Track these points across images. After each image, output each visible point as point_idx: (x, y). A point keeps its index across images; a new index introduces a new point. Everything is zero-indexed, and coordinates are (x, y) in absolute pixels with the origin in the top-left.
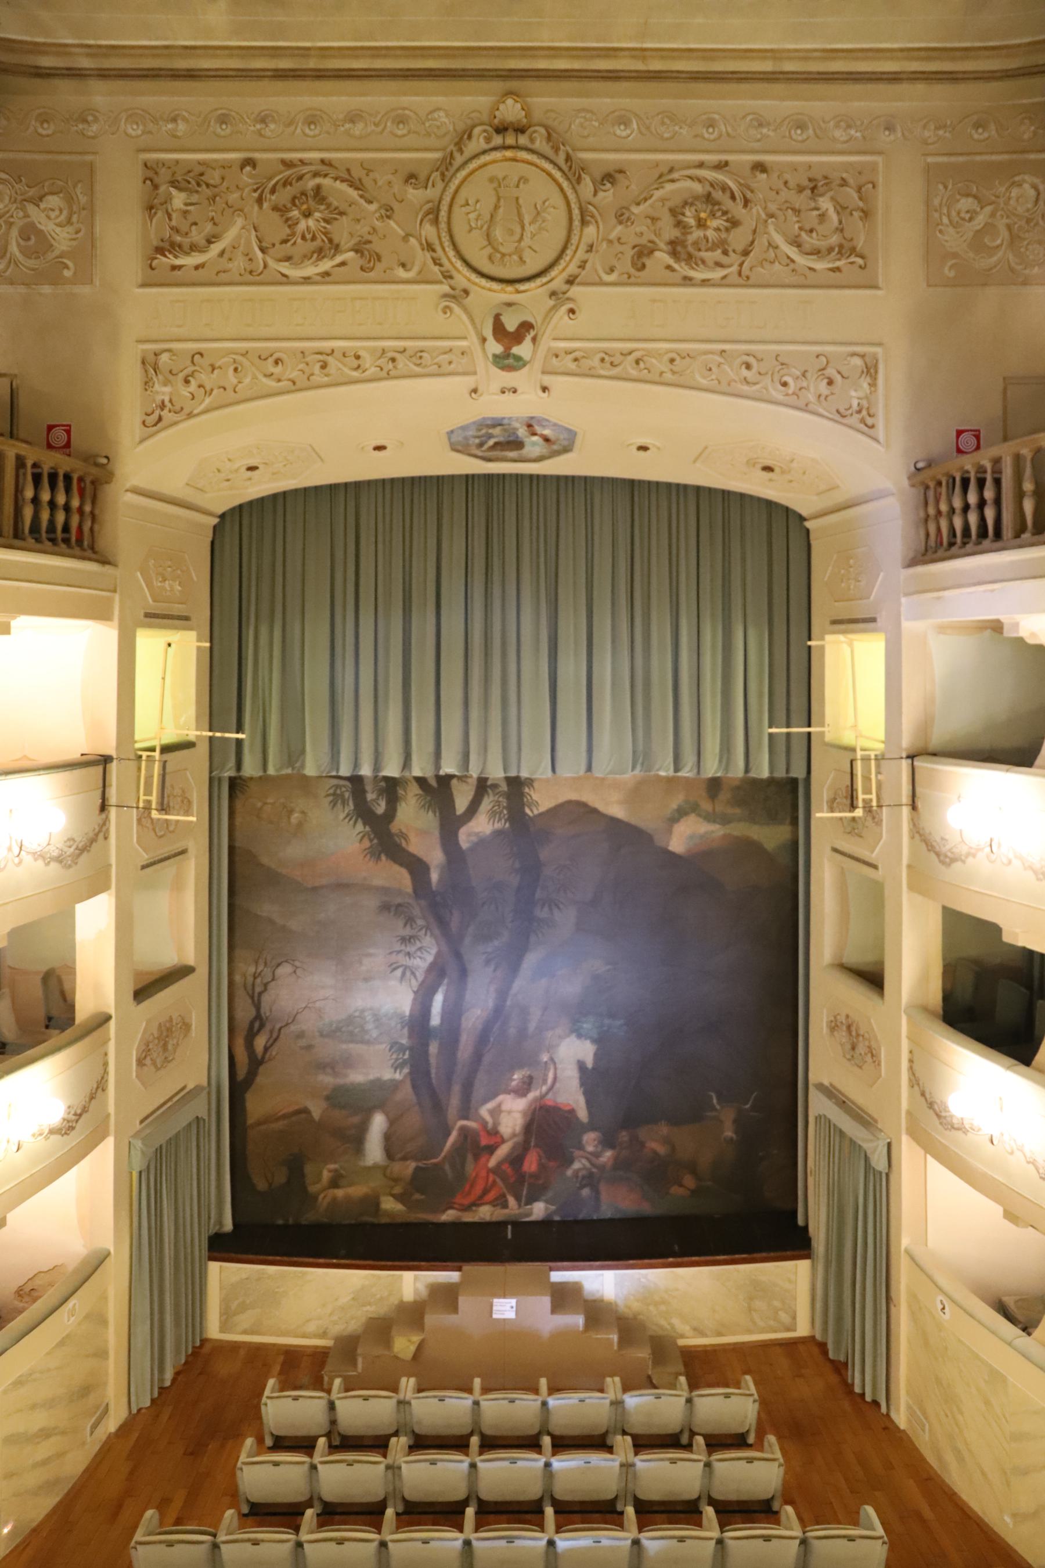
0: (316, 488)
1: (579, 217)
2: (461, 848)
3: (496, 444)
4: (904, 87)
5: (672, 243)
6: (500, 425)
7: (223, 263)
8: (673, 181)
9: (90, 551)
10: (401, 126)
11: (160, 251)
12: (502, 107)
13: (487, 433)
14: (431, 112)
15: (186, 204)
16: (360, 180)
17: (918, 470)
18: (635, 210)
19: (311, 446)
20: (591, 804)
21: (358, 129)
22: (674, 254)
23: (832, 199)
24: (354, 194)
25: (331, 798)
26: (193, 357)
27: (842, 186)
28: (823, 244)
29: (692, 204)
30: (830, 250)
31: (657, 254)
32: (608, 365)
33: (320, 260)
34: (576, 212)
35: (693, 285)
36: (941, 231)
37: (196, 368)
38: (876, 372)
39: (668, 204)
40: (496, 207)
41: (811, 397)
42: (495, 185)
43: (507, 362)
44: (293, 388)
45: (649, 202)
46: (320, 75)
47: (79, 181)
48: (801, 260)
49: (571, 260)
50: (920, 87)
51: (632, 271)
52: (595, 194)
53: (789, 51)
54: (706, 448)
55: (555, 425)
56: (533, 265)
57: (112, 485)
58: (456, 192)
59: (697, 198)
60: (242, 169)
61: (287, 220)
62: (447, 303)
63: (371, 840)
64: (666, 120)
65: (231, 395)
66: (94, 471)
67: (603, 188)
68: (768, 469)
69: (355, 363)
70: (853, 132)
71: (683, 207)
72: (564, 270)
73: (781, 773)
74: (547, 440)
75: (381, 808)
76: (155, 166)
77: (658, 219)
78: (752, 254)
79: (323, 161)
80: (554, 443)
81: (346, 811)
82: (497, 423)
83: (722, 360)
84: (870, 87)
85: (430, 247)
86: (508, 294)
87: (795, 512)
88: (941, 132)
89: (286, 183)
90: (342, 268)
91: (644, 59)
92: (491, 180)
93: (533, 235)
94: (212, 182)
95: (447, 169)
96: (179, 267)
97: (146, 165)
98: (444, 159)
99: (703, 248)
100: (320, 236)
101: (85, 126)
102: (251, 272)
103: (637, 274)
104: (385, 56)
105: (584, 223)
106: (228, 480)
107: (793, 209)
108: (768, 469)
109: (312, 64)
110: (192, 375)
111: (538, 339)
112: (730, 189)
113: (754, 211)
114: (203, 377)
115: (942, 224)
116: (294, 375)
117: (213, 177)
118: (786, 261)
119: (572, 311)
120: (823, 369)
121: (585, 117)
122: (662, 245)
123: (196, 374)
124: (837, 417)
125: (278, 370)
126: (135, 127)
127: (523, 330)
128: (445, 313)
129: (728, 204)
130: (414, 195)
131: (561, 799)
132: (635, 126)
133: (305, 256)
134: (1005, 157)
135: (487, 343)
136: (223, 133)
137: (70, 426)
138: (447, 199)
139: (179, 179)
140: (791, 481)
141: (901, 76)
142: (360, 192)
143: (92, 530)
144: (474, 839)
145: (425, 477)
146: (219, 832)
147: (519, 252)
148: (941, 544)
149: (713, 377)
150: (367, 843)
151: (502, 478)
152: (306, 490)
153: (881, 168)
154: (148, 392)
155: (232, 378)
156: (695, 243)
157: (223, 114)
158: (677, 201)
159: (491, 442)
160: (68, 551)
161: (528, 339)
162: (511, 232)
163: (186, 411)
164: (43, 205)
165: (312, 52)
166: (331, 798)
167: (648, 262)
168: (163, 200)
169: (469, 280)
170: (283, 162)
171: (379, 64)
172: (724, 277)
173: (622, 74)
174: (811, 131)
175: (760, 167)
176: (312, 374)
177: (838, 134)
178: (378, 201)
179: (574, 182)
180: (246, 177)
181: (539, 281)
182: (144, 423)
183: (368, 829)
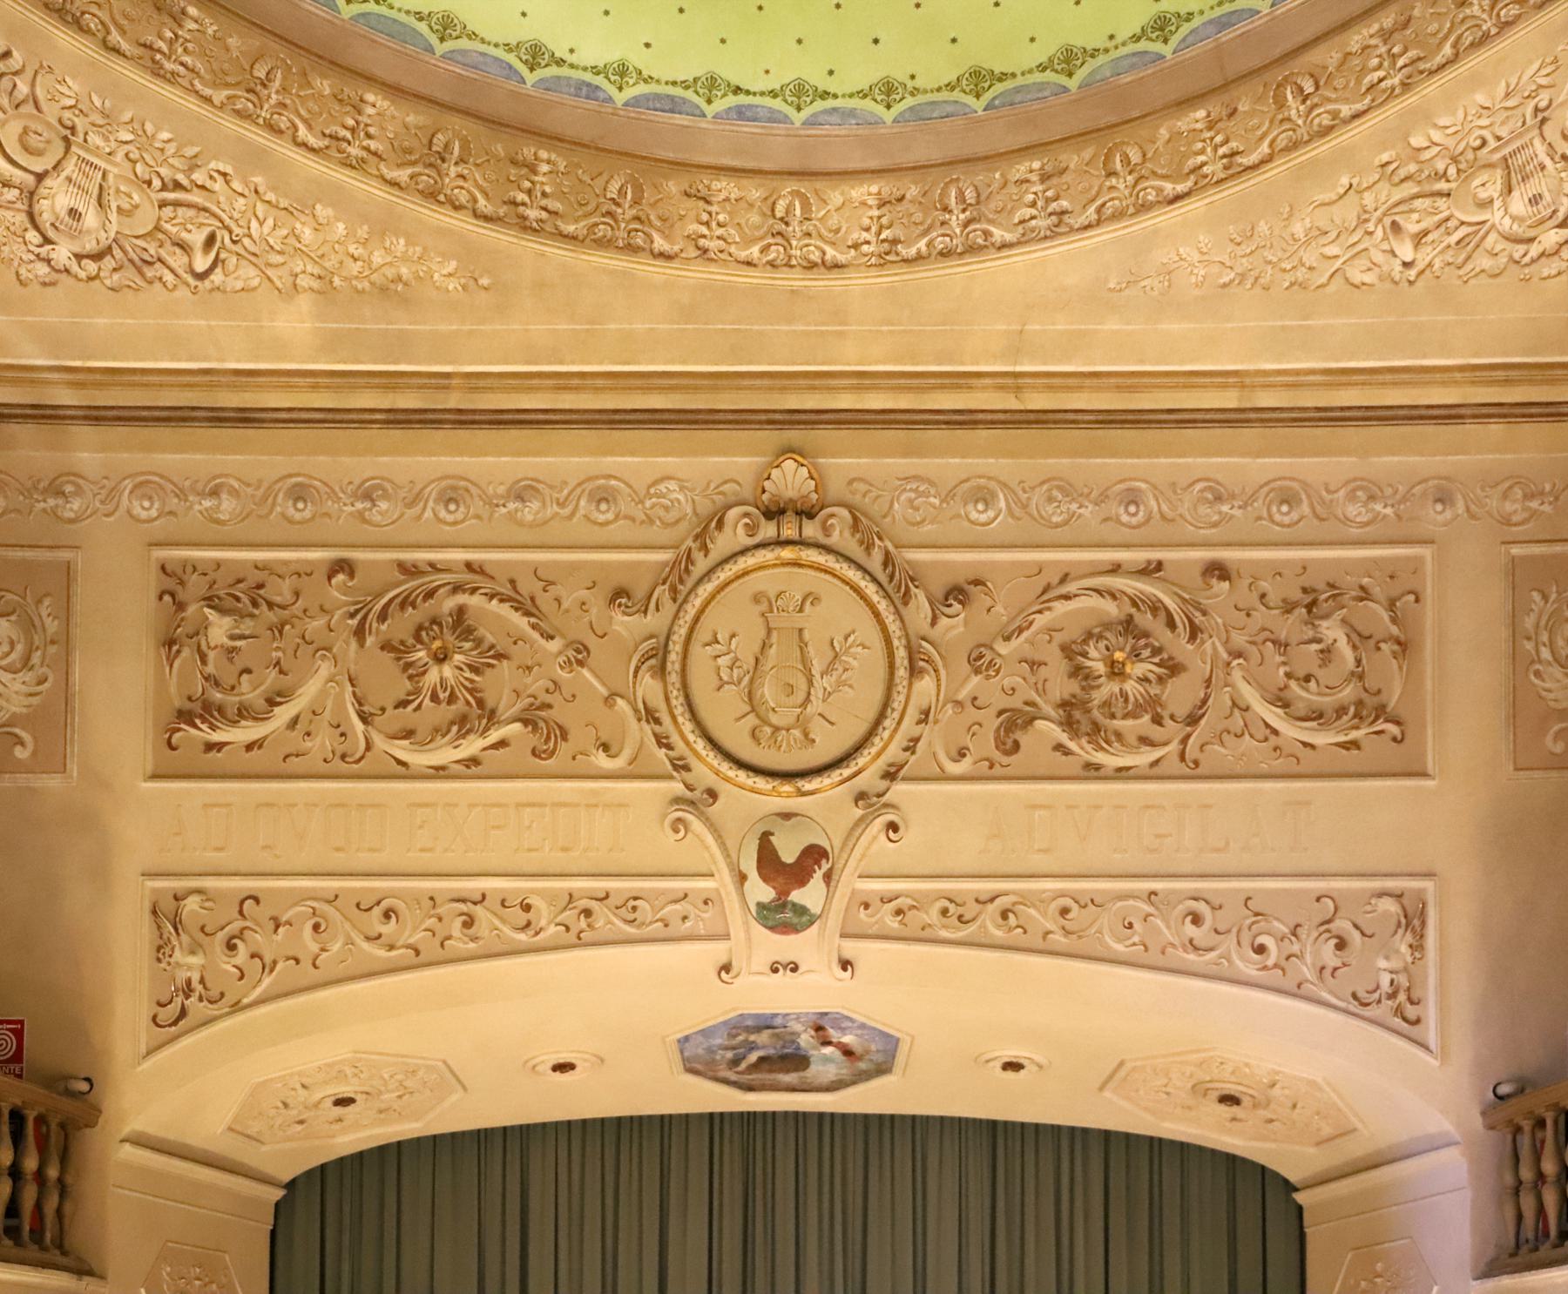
0: (455, 1138)
1: (906, 662)
3: (762, 1060)
4: (1471, 429)
5: (1064, 705)
6: (768, 1027)
7: (295, 740)
8: (1067, 597)
9: (57, 1252)
10: (603, 506)
11: (186, 717)
13: (746, 1041)
14: (655, 483)
15: (233, 638)
16: (532, 599)
17: (1500, 1098)
18: (1003, 648)
19: (445, 1062)
21: (530, 511)
22: (1069, 724)
23: (1344, 621)
24: (521, 622)
26: (242, 902)
27: (1362, 599)
28: (1327, 701)
29: (1100, 637)
30: (1341, 711)
31: (1039, 724)
32: (954, 920)
33: (464, 737)
34: (901, 654)
35: (1105, 778)
36: (1537, 674)
37: (248, 924)
38: (1423, 924)
39: (1059, 638)
41: (1308, 973)
42: (764, 607)
44: (416, 961)
45: (1025, 634)
46: (465, 419)
47: (46, 595)
48: (1291, 731)
49: (891, 737)
50: (1496, 429)
51: (997, 756)
52: (934, 622)
53: (1265, 373)
54: (1121, 1064)
55: (863, 1026)
56: (827, 745)
57: (97, 1129)
58: (697, 619)
59: (1107, 626)
60: (329, 579)
62: (680, 814)
64: (1057, 494)
65: (307, 973)
66: (67, 1105)
67: (947, 610)
68: (1229, 1099)
69: (523, 918)
70: (1378, 507)
71: (1085, 642)
72: (879, 754)
74: (848, 1052)
76: (179, 571)
78: (1203, 722)
79: (469, 566)
80: (860, 1058)
82: (764, 1024)
83: (1151, 909)
85: (651, 716)
86: (781, 797)
87: (1276, 1175)
88: (1534, 504)
89: (406, 602)
91: (1018, 389)
92: (757, 599)
93: (827, 695)
94: (278, 599)
95: (681, 581)
96: (219, 746)
97: (163, 568)
98: (676, 562)
99: (1119, 715)
100: (463, 694)
101: (60, 501)
102: (343, 757)
103: (1005, 760)
105: (914, 672)
106: (301, 1122)
107: (1274, 642)
108: (1229, 1099)
109: (454, 401)
110: (240, 935)
111: (835, 877)
112: (1166, 609)
113: (1208, 645)
114: (258, 939)
115: (1540, 661)
116: (417, 937)
117: (281, 591)
118: (1262, 732)
119: (893, 827)
120: (1328, 922)
121: (916, 490)
122: (1048, 710)
123: (246, 932)
124: (1353, 1006)
125: (388, 929)
126: (146, 504)
127: (810, 861)
128: (676, 831)
129: (1162, 635)
130: (624, 624)
132: (1002, 504)
133: (437, 730)
135: (747, 884)
136: (298, 516)
137: (21, 1022)
138: (681, 631)
139: (221, 593)
140: (1271, 1121)
141: (1463, 411)
142: (533, 620)
143: (59, 1212)
145: (641, 1118)
147: (802, 723)
148: (1547, 1235)
149: (1136, 939)
151: (770, 1119)
152: (435, 1139)
153: (1429, 567)
154: (163, 965)
156: (1106, 704)
157: (297, 485)
158: (1073, 633)
159: (753, 1057)
160: (15, 1251)
161: (818, 875)
162: (790, 689)
163: (230, 998)
165: (454, 382)
167: (1025, 739)
168: (191, 630)
169: (717, 773)
170: (402, 566)
171: (567, 401)
172: (1156, 763)
173: (981, 416)
174: (1305, 508)
175: (1217, 570)
176: (449, 938)
177: (1352, 510)
178: (563, 636)
179: (897, 602)
180: (337, 592)
181: (836, 776)
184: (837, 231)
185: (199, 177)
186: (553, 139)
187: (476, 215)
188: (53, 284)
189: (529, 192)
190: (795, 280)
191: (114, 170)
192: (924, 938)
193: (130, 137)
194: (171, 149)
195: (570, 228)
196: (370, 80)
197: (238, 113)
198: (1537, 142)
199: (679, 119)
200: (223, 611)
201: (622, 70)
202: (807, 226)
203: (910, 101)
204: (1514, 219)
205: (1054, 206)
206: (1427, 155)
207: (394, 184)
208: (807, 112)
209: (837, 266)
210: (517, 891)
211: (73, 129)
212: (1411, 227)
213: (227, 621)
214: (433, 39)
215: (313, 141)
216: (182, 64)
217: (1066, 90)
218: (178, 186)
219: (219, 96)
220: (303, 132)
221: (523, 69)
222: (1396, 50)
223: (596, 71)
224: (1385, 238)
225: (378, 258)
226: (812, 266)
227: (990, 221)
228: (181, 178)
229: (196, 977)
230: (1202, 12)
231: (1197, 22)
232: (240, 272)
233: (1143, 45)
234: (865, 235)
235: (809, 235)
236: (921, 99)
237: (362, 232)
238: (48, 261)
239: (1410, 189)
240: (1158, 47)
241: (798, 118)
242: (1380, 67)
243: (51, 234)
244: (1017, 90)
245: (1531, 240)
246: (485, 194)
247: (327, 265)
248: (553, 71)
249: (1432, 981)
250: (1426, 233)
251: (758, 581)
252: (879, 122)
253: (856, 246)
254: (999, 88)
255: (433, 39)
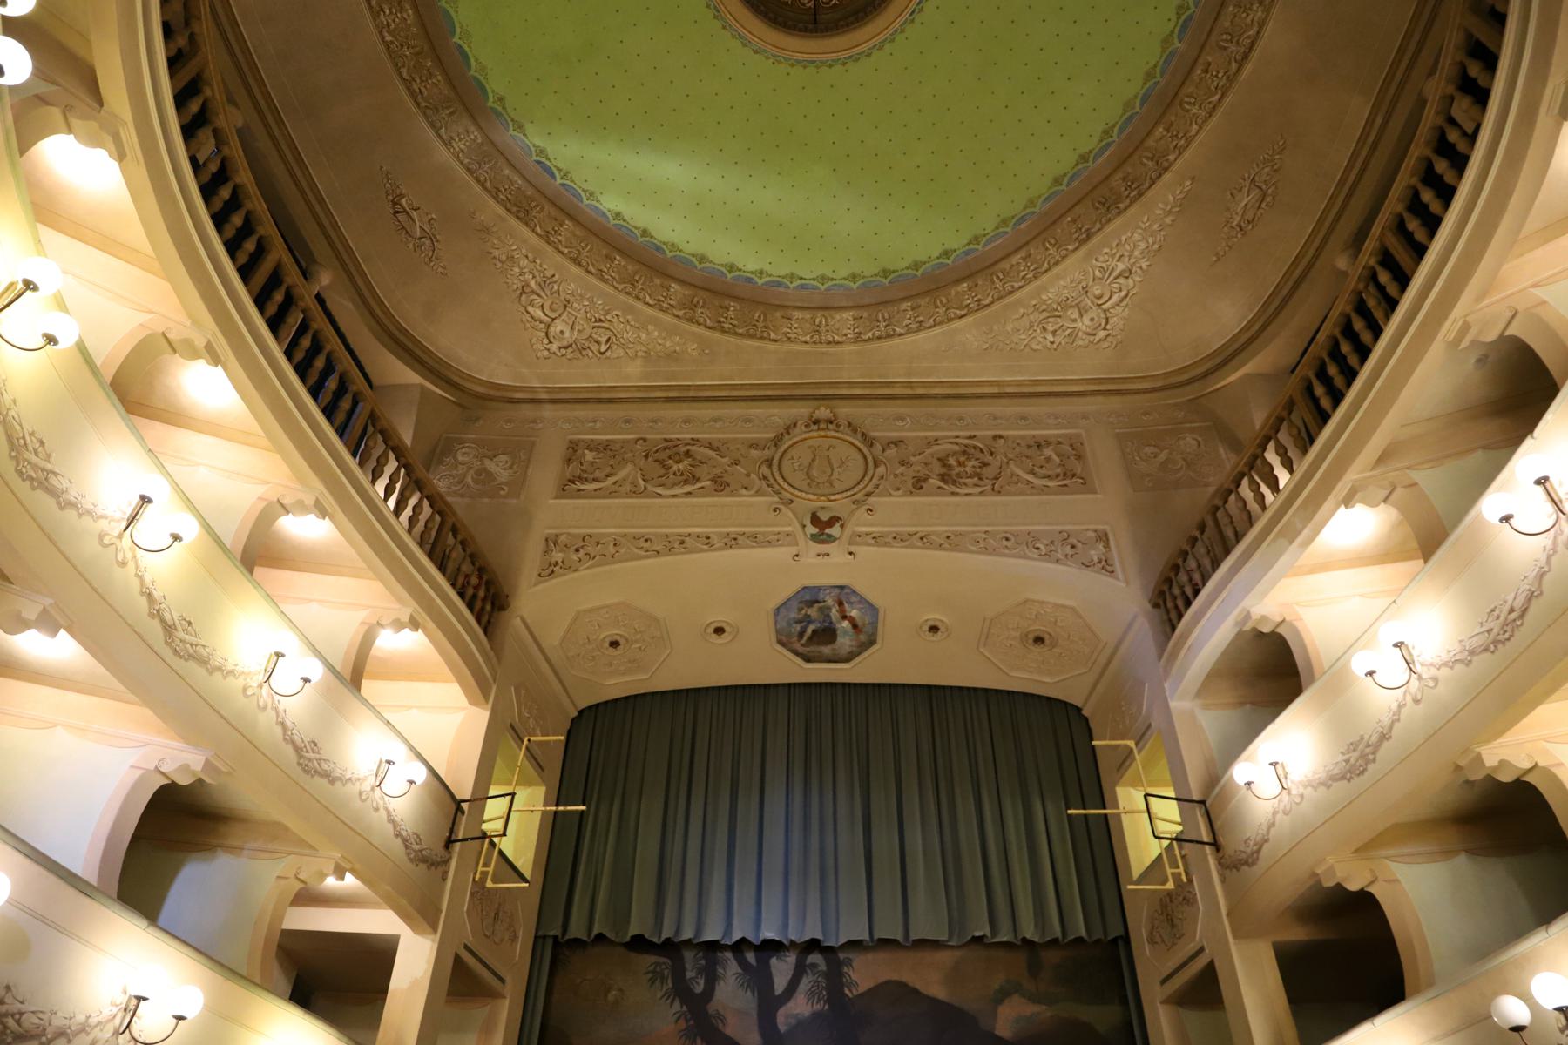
2: (779, 1031)
12: (817, 412)
18: (912, 459)
20: (911, 984)
24: (713, 454)
25: (650, 975)
30: (1058, 476)
31: (931, 481)
40: (813, 460)
42: (813, 449)
45: (922, 455)
48: (1037, 482)
49: (867, 484)
52: (884, 451)
57: (507, 612)
61: (664, 466)
63: (687, 1021)
73: (1098, 934)
75: (699, 987)
77: (929, 464)
81: (664, 990)
84: (1066, 399)
85: (765, 478)
90: (701, 490)
91: (912, 388)
92: (810, 447)
94: (614, 448)
104: (740, 390)
105: (876, 465)
109: (692, 394)
110: (582, 547)
113: (998, 457)
131: (882, 979)
134: (1170, 427)
135: (806, 529)
144: (793, 1021)
146: (536, 992)
150: (682, 1024)
155: (612, 550)
161: (838, 525)
164: (495, 460)
165: (692, 388)
166: (650, 975)
171: (735, 393)
174: (1031, 421)
182: (540, 575)
183: (685, 1008)
184: (838, 330)
185: (608, 317)
186: (736, 298)
187: (706, 327)
188: (549, 358)
189: (726, 318)
190: (823, 348)
191: (579, 316)
193: (587, 303)
194: (601, 307)
195: (740, 331)
197: (627, 293)
198: (1086, 299)
199: (782, 290)
200: (591, 450)
201: (761, 272)
202: (828, 328)
203: (862, 281)
204: (1087, 326)
205: (917, 320)
206: (1049, 302)
207: (678, 316)
208: (826, 285)
209: (838, 343)
211: (569, 302)
212: (1050, 328)
215: (651, 302)
216: (611, 276)
217: (916, 275)
218: (601, 321)
219: (621, 287)
220: (648, 299)
221: (727, 273)
222: (1029, 264)
223: (752, 273)
224: (1041, 332)
225: (668, 344)
226: (829, 343)
227: (895, 325)
228: (602, 318)
229: (560, 561)
230: (959, 249)
231: (958, 252)
232: (618, 351)
233: (941, 260)
234: (849, 331)
235: (828, 331)
236: (865, 280)
238: (548, 350)
239: (1045, 314)
240: (946, 261)
242: (1024, 270)
243: (552, 340)
244: (900, 276)
245: (1095, 335)
246: (710, 319)
247: (649, 347)
248: (737, 273)
250: (1056, 331)
251: (810, 442)
252: (852, 289)
253: (846, 335)
254: (892, 276)
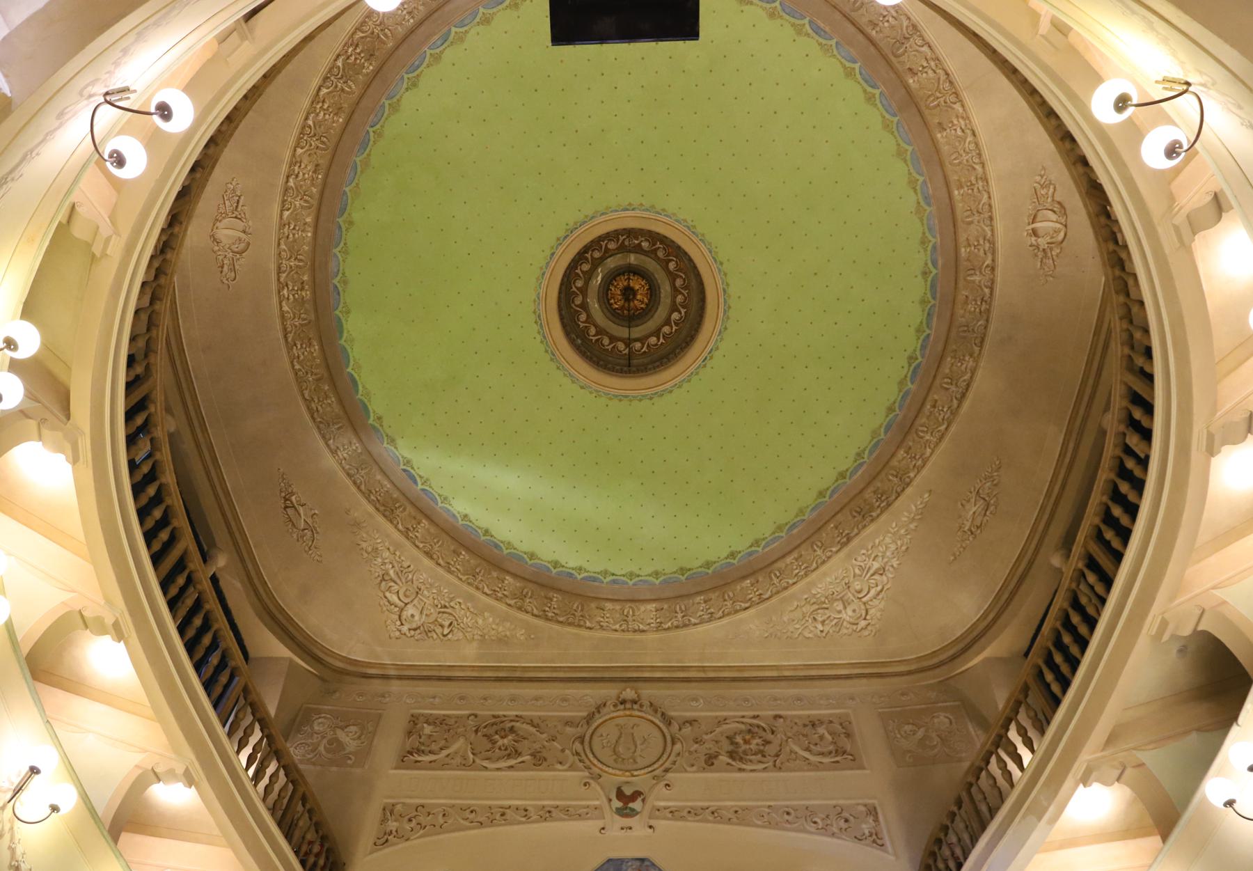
5: (728, 752)
18: (705, 737)
24: (533, 730)
28: (825, 750)
29: (740, 734)
30: (830, 753)
31: (721, 757)
32: (693, 815)
40: (620, 737)
43: (625, 812)
46: (520, 680)
48: (813, 759)
50: (864, 681)
51: (705, 766)
72: (662, 765)
79: (517, 716)
83: (770, 811)
85: (578, 754)
88: (883, 699)
89: (493, 724)
91: (704, 671)
92: (617, 725)
96: (419, 761)
109: (518, 674)
110: (415, 817)
113: (778, 735)
119: (667, 785)
130: (569, 730)
138: (590, 731)
155: (441, 820)
161: (639, 800)
164: (346, 730)
171: (555, 675)
185: (452, 604)
186: (559, 590)
187: (533, 615)
189: (550, 607)
190: (630, 636)
192: (682, 818)
194: (446, 595)
195: (561, 619)
196: (508, 572)
199: (596, 584)
201: (580, 569)
205: (709, 611)
206: (818, 596)
207: (509, 605)
210: (522, 805)
211: (420, 589)
212: (820, 619)
213: (431, 727)
214: (528, 560)
215: (489, 592)
217: (708, 573)
218: (445, 607)
219: (464, 578)
223: (573, 569)
228: (447, 604)
229: (394, 829)
231: (742, 553)
233: (728, 560)
237: (497, 621)
239: (816, 607)
241: (631, 583)
243: (404, 622)
244: (694, 573)
248: (561, 569)
249: (885, 832)
253: (649, 624)
254: (689, 573)
255: (528, 560)
